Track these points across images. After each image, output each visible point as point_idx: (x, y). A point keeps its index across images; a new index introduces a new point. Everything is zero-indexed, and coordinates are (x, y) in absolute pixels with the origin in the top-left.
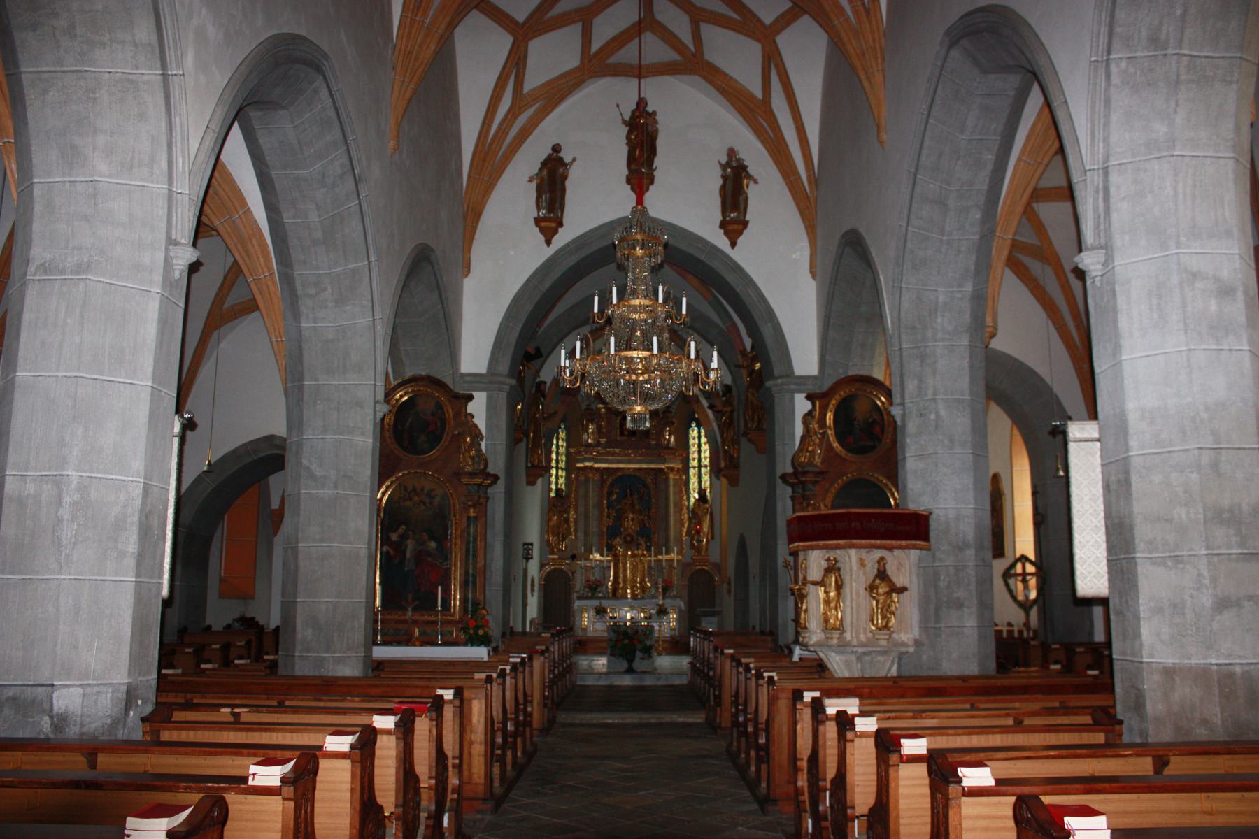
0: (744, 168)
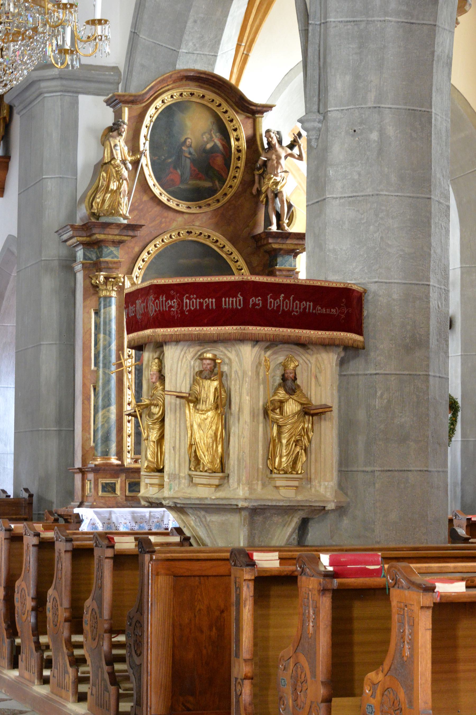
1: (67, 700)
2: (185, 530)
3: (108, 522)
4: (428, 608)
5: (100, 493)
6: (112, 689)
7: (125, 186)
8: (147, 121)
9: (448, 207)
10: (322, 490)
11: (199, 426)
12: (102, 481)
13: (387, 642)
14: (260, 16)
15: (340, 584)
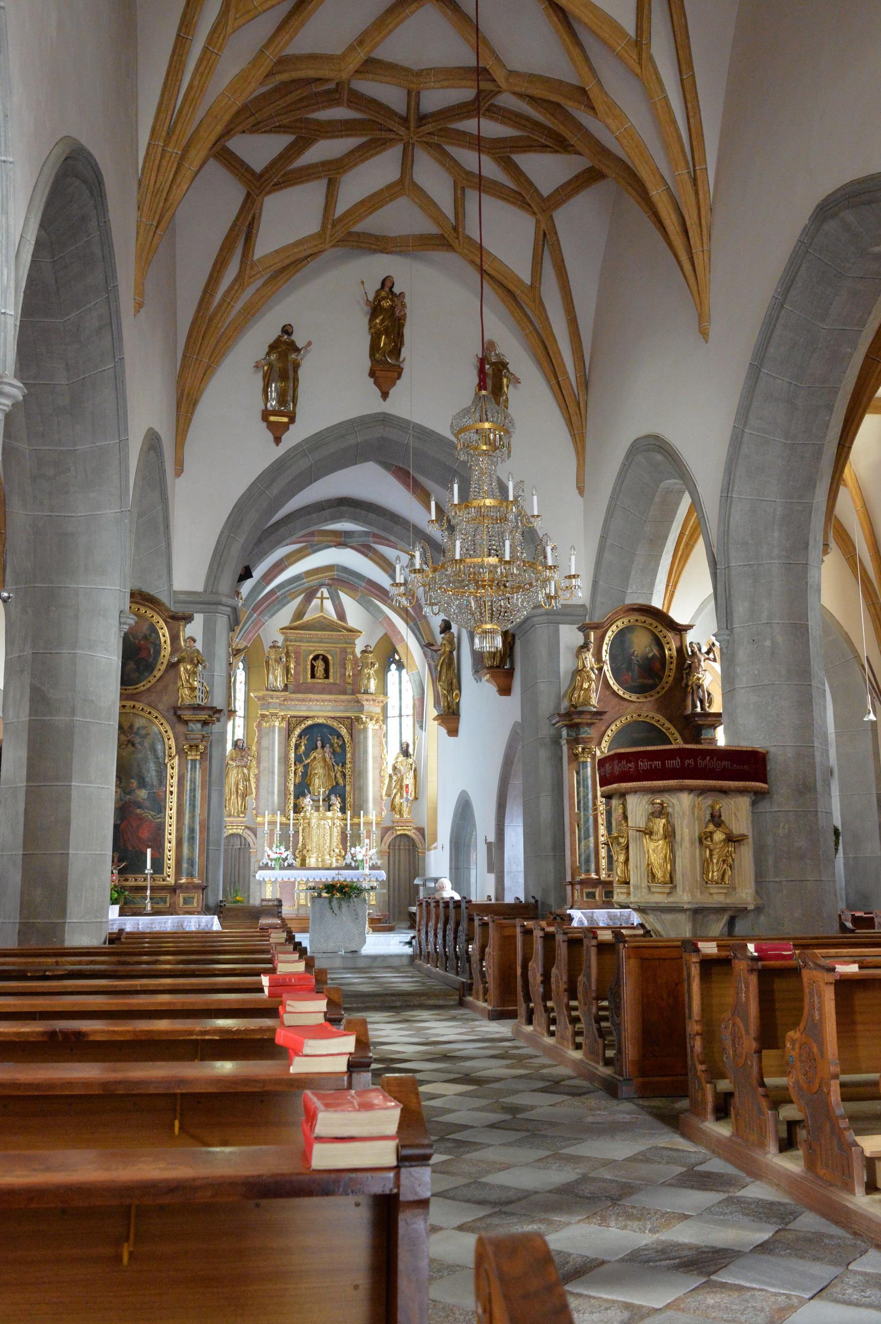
0: (504, 365)
1: (568, 1048)
2: (646, 925)
3: (591, 919)
4: (831, 983)
5: (585, 899)
6: (600, 1041)
7: (593, 685)
8: (607, 640)
9: (825, 691)
10: (744, 896)
11: (654, 851)
12: (586, 890)
13: (801, 1009)
14: (682, 562)
15: (763, 966)
